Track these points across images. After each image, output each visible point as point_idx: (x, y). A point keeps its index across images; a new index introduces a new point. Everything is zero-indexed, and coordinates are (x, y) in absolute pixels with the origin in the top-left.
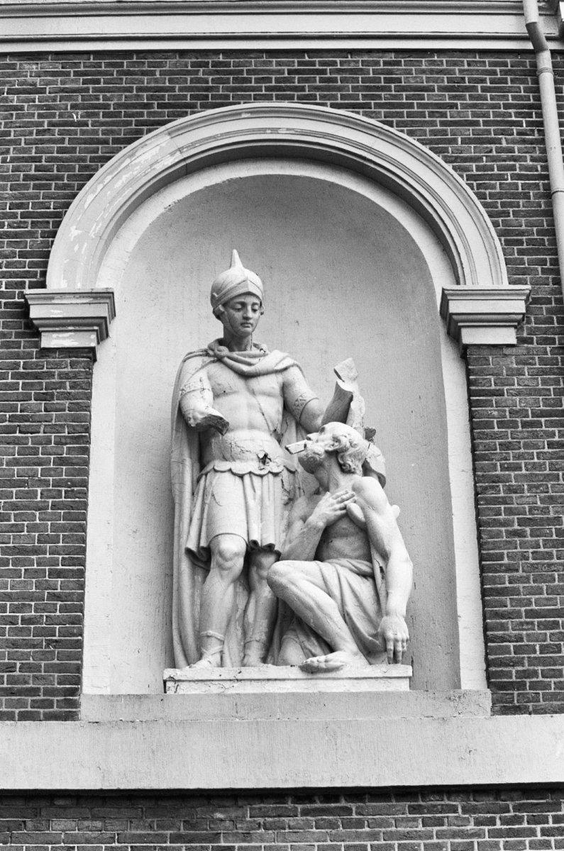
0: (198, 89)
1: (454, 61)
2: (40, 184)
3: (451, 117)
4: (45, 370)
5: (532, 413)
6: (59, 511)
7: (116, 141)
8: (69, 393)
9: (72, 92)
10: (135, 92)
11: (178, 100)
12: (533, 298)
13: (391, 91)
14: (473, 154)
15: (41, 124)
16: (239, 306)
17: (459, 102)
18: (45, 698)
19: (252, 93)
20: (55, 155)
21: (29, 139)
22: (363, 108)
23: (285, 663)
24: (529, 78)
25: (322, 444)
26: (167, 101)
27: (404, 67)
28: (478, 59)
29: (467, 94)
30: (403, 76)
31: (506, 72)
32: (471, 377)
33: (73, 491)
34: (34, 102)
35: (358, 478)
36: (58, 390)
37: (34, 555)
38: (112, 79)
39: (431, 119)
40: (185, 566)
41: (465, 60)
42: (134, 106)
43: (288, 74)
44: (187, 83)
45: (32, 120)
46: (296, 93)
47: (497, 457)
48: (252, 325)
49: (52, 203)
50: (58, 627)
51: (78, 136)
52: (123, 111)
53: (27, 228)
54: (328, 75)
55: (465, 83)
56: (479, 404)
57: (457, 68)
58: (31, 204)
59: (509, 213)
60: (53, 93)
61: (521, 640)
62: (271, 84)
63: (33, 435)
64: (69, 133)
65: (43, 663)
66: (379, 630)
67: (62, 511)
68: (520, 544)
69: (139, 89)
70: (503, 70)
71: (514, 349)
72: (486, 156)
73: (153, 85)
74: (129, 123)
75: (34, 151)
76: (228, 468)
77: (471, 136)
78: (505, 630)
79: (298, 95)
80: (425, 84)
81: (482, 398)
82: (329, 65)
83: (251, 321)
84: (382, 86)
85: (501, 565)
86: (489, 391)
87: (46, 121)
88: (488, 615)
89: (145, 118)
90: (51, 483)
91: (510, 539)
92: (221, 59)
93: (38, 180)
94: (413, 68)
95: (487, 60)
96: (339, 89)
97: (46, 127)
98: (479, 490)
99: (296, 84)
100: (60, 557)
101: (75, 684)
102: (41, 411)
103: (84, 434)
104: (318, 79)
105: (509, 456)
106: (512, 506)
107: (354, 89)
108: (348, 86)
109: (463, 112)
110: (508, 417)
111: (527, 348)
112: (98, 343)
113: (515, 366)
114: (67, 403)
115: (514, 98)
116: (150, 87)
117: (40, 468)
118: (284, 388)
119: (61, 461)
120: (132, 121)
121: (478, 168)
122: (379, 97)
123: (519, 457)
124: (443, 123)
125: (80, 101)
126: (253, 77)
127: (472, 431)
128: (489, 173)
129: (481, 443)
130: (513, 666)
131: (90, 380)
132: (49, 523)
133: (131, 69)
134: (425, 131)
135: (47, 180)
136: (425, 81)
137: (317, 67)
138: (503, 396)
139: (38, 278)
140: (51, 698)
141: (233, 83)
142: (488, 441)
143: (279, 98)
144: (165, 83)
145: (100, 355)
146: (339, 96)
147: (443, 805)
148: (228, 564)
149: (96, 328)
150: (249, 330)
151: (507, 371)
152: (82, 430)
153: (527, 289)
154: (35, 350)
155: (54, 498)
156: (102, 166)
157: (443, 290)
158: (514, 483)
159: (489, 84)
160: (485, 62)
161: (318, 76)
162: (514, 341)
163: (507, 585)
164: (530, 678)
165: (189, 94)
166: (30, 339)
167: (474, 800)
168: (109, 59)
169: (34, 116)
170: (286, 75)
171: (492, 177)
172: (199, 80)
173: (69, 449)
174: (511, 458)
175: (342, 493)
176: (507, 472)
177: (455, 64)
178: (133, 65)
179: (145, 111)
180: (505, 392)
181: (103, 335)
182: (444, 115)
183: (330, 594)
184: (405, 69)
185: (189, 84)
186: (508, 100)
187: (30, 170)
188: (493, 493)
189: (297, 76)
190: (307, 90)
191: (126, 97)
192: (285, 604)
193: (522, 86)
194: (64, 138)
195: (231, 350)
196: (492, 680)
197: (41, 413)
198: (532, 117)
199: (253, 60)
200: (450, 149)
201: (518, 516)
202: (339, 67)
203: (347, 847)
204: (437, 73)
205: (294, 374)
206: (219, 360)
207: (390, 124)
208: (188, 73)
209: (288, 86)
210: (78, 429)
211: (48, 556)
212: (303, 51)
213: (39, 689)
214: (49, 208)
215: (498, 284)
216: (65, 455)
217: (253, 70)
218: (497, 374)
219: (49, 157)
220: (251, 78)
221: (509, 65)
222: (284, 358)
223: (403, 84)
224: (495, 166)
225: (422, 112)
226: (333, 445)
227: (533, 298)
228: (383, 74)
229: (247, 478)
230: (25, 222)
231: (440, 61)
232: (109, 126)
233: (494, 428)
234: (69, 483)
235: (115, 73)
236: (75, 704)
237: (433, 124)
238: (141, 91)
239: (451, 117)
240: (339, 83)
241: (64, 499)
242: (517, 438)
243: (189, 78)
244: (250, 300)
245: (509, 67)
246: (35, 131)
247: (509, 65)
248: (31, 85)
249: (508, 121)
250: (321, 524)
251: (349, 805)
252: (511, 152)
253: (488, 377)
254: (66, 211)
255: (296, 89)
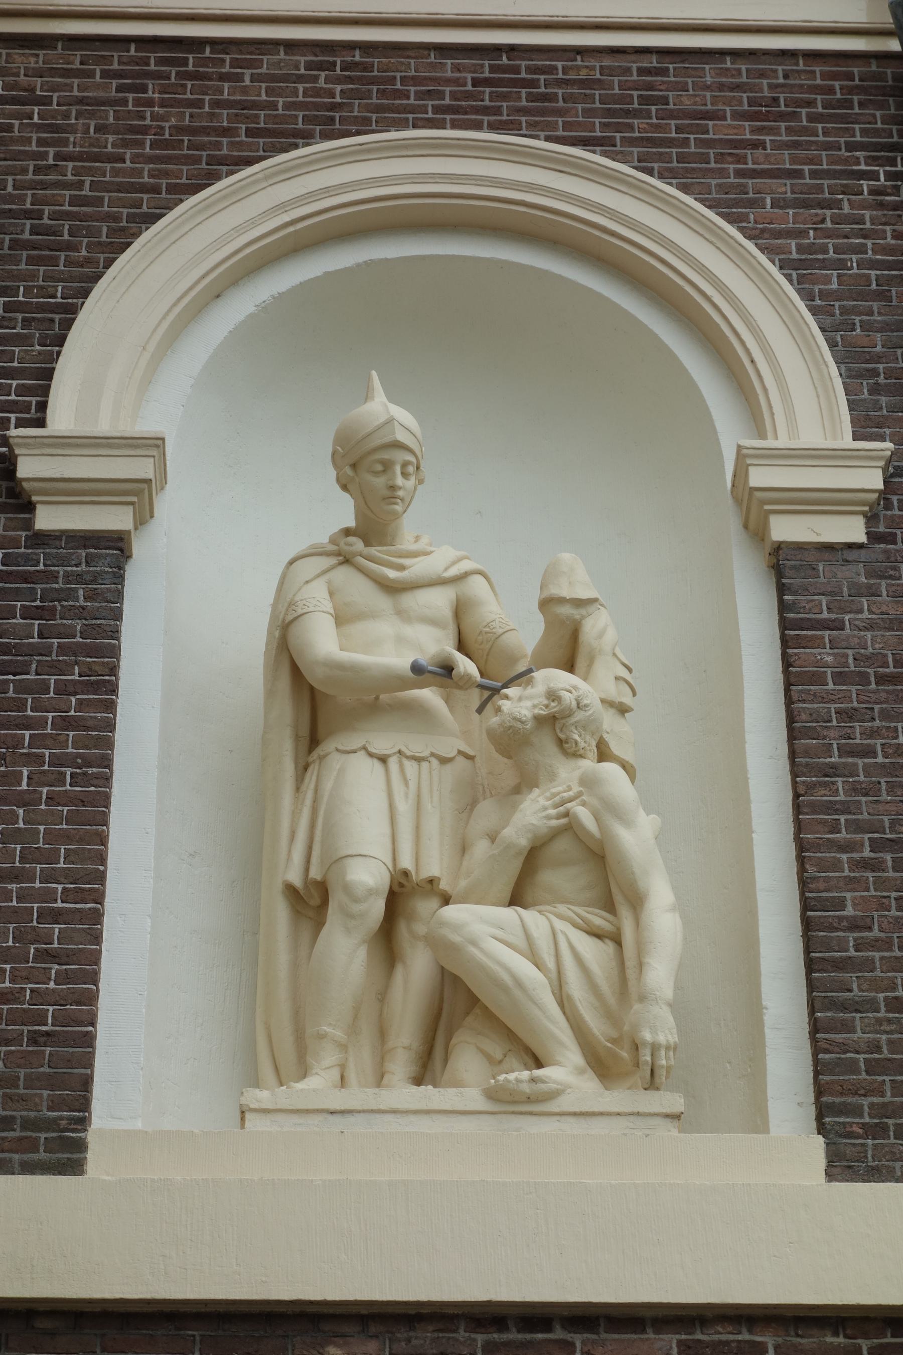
0: (317, 107)
1: (759, 69)
2: (39, 256)
3: (753, 164)
4: (41, 567)
5: (895, 660)
6: (60, 808)
7: (171, 189)
8: (83, 608)
9: (97, 105)
10: (207, 109)
11: (281, 124)
12: (895, 467)
13: (651, 118)
14: (791, 225)
15: (44, 156)
16: (379, 468)
17: (768, 138)
18: (24, 1134)
19: (411, 116)
20: (67, 208)
21: (21, 180)
22: (602, 145)
23: (458, 1084)
24: (891, 100)
25: (529, 704)
26: (262, 125)
27: (672, 79)
28: (801, 66)
29: (783, 125)
30: (670, 94)
31: (851, 90)
32: (786, 597)
33: (85, 774)
34: (32, 119)
35: (588, 764)
36: (64, 603)
37: (12, 883)
38: (168, 85)
39: (719, 166)
40: (281, 912)
41: (780, 68)
42: (205, 131)
43: (474, 85)
44: (297, 97)
45: (27, 148)
46: (486, 118)
47: (832, 733)
48: (402, 500)
49: (60, 288)
50: (51, 1008)
51: (107, 179)
52: (186, 138)
53: (14, 328)
54: (542, 90)
55: (779, 106)
56: (800, 643)
57: (765, 82)
58: (22, 289)
59: (854, 324)
60: (64, 105)
61: (879, 1049)
62: (443, 102)
63: (18, 677)
64: (90, 172)
65: (22, 1073)
66: (626, 1028)
67: (66, 809)
68: (874, 883)
69: (216, 104)
70: (847, 86)
71: (863, 551)
72: (815, 229)
73: (239, 98)
74: (198, 160)
75: (29, 200)
76: (360, 745)
77: (789, 195)
78: (849, 1032)
79: (489, 122)
80: (709, 107)
81: (805, 632)
82: (544, 73)
83: (400, 493)
84: (635, 110)
85: (841, 919)
86: (818, 621)
87: (51, 151)
88: (817, 1004)
89: (225, 151)
90: (47, 759)
91: (857, 874)
92: (357, 58)
93: (35, 248)
94: (689, 80)
95: (817, 69)
96: (559, 112)
97: (51, 162)
98: (801, 790)
99: (487, 103)
100: (60, 887)
101: (79, 1111)
102: (33, 638)
103: (107, 678)
104: (524, 96)
105: (854, 733)
106: (860, 817)
107: (587, 113)
108: (576, 108)
109: (775, 155)
110: (852, 666)
111: (886, 551)
112: (136, 529)
113: (863, 580)
114: (78, 625)
115: (864, 132)
116: (235, 101)
117: (27, 734)
118: (460, 610)
119: (66, 723)
120: (201, 156)
121: (800, 249)
122: (631, 128)
123: (873, 733)
124: (740, 174)
125: (111, 120)
126: (412, 89)
127: (787, 691)
128: (820, 257)
129: (804, 708)
130: (865, 1096)
131: (120, 586)
132: (42, 828)
133: (201, 69)
134: (709, 185)
135: (52, 250)
136: (709, 103)
137: (524, 75)
138: (843, 629)
139: (33, 414)
140: (34, 1135)
141: (378, 98)
142: (815, 706)
143: (455, 125)
144: (259, 95)
145: (138, 548)
146: (560, 124)
147: (739, 1342)
148: (356, 908)
149: (135, 499)
150: (399, 508)
151: (849, 589)
152: (107, 671)
153: (887, 449)
154: (24, 534)
155: (51, 786)
156: (147, 229)
157: (739, 448)
158: (862, 778)
159: (820, 110)
160: (814, 72)
161: (524, 91)
162: (862, 538)
163: (852, 953)
164: (895, 1118)
165: (301, 114)
166: (15, 516)
167: (798, 1335)
168: (164, 52)
169: (30, 143)
170: (469, 87)
171: (824, 265)
172: (318, 92)
173: (80, 702)
174: (858, 735)
175: (560, 789)
176: (850, 760)
177: (762, 75)
178: (204, 62)
179: (225, 140)
180: (847, 623)
181: (145, 514)
182: (741, 159)
183: (538, 964)
184: (676, 82)
185: (301, 98)
186: (854, 136)
187: (23, 231)
188: (825, 795)
189: (488, 90)
190: (505, 113)
191: (191, 116)
192: (456, 980)
193: (878, 114)
194: (83, 181)
195: (367, 544)
196: (827, 1119)
197: (31, 640)
198: (896, 166)
199: (412, 61)
200: (752, 216)
201: (871, 835)
202: (560, 76)
203: (489, 1347)
204: (732, 89)
205: (478, 587)
206: (347, 560)
207: (650, 172)
208: (300, 79)
209: (472, 106)
210: (97, 668)
211: (37, 885)
212: (497, 49)
213: (13, 1118)
214: (54, 297)
215: (835, 438)
216: (72, 713)
217: (413, 78)
218: (832, 594)
219: (54, 212)
220: (408, 91)
221: (857, 79)
222: (460, 560)
223: (671, 106)
224: (831, 246)
225: (703, 154)
226: (547, 706)
227: (895, 467)
228: (637, 90)
229: (393, 763)
230: (11, 319)
231: (735, 69)
232: (162, 163)
233: (827, 684)
234: (79, 761)
235: (173, 75)
236: (80, 1146)
237: (723, 173)
238: (218, 107)
239: (753, 164)
240: (561, 103)
241: (68, 788)
242: (870, 702)
243: (301, 87)
244: (402, 456)
245: (857, 82)
246: (31, 168)
247: (857, 79)
248: (25, 90)
249: (853, 172)
250: (524, 842)
251: (569, 1337)
252: (857, 223)
253: (816, 597)
254: (83, 303)
255: (486, 111)
